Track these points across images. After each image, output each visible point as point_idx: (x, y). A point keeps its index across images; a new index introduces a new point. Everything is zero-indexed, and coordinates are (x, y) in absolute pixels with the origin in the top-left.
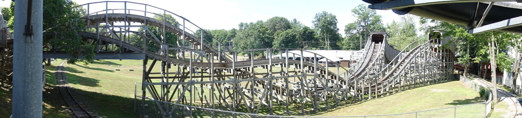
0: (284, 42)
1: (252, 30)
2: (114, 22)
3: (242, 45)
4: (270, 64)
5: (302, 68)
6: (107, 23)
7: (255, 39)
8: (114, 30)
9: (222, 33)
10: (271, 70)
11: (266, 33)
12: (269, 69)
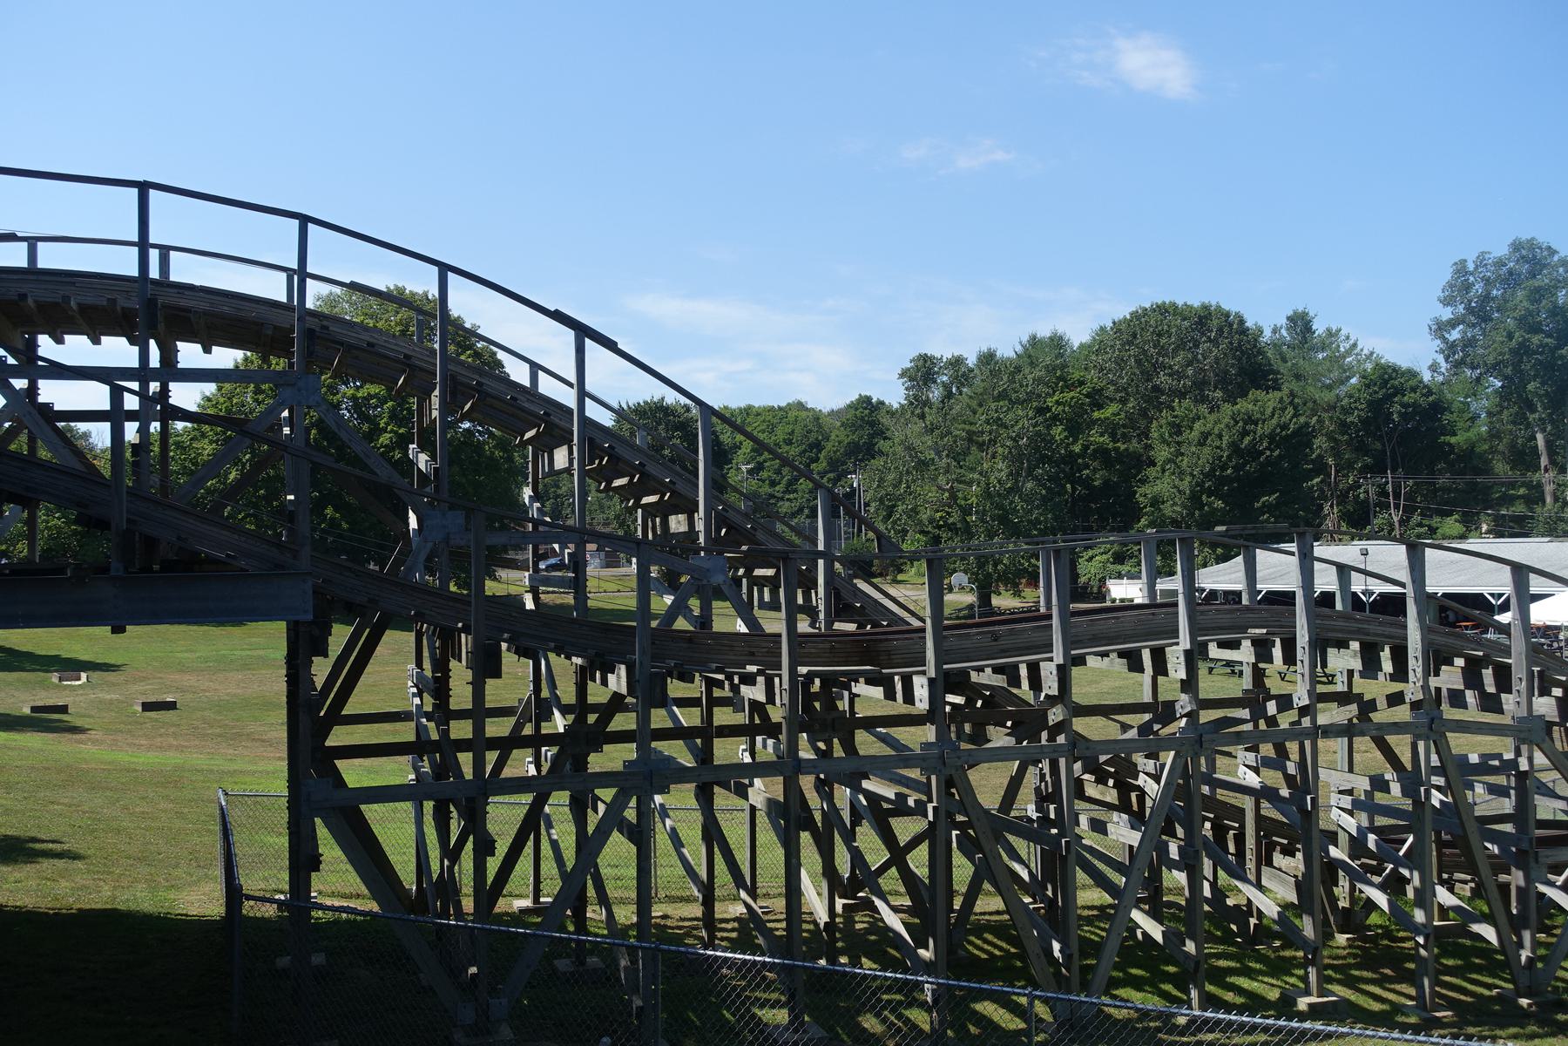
0: (1223, 481)
1: (993, 406)
5: (1419, 670)
8: (41, 399)
9: (789, 429)
11: (1094, 422)
12: (1177, 669)
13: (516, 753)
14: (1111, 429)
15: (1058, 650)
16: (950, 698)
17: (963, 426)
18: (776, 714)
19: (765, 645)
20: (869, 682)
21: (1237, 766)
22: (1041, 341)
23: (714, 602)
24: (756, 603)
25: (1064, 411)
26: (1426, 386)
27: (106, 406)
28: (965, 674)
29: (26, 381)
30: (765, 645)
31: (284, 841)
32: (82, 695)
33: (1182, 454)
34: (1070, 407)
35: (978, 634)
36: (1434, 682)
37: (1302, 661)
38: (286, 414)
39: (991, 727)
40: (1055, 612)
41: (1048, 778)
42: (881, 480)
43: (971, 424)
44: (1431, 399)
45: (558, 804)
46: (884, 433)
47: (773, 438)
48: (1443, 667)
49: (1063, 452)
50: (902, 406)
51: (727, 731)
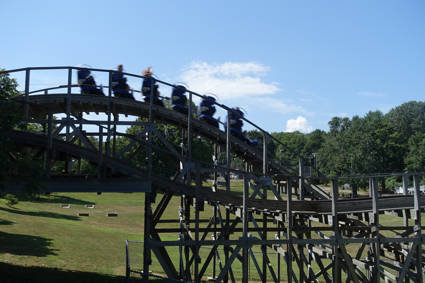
1: (357, 133)
2: (84, 113)
3: (336, 166)
4: (416, 208)
6: (68, 115)
7: (365, 150)
8: (83, 130)
11: (390, 138)
12: (414, 217)
13: (209, 233)
14: (396, 140)
15: (374, 209)
16: (340, 222)
19: (282, 204)
20: (314, 217)
24: (281, 191)
25: (380, 134)
27: (98, 132)
28: (345, 215)
29: (79, 125)
30: (282, 204)
31: (142, 255)
32: (92, 211)
33: (419, 149)
34: (382, 133)
35: (348, 203)
38: (147, 134)
39: (354, 232)
40: (374, 197)
41: (372, 249)
42: (322, 155)
43: (351, 138)
45: (221, 248)
47: (290, 142)
50: (329, 132)
51: (270, 230)
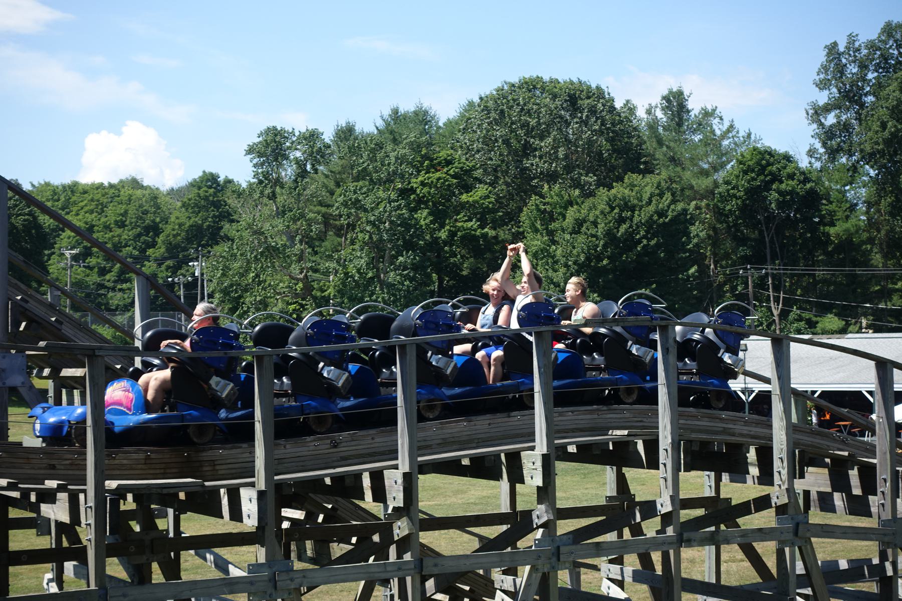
1: (351, 186)
5: (784, 472)
7: (377, 250)
9: (121, 209)
10: (546, 493)
11: (463, 206)
12: (534, 477)
16: (287, 512)
17: (319, 208)
18: (87, 534)
21: (601, 579)
22: (405, 116)
23: (9, 409)
25: (429, 193)
26: (803, 173)
36: (800, 485)
37: (665, 465)
39: (335, 544)
42: (226, 269)
43: (328, 206)
44: (808, 186)
46: (231, 215)
47: (103, 220)
48: (811, 469)
49: (428, 238)
